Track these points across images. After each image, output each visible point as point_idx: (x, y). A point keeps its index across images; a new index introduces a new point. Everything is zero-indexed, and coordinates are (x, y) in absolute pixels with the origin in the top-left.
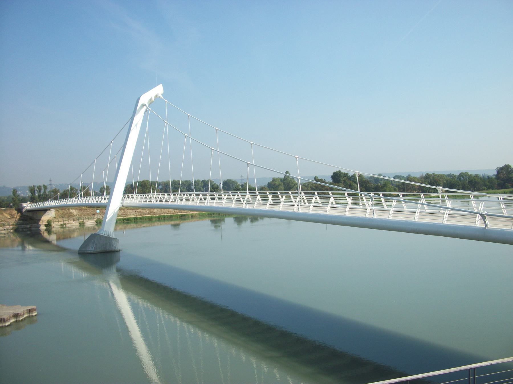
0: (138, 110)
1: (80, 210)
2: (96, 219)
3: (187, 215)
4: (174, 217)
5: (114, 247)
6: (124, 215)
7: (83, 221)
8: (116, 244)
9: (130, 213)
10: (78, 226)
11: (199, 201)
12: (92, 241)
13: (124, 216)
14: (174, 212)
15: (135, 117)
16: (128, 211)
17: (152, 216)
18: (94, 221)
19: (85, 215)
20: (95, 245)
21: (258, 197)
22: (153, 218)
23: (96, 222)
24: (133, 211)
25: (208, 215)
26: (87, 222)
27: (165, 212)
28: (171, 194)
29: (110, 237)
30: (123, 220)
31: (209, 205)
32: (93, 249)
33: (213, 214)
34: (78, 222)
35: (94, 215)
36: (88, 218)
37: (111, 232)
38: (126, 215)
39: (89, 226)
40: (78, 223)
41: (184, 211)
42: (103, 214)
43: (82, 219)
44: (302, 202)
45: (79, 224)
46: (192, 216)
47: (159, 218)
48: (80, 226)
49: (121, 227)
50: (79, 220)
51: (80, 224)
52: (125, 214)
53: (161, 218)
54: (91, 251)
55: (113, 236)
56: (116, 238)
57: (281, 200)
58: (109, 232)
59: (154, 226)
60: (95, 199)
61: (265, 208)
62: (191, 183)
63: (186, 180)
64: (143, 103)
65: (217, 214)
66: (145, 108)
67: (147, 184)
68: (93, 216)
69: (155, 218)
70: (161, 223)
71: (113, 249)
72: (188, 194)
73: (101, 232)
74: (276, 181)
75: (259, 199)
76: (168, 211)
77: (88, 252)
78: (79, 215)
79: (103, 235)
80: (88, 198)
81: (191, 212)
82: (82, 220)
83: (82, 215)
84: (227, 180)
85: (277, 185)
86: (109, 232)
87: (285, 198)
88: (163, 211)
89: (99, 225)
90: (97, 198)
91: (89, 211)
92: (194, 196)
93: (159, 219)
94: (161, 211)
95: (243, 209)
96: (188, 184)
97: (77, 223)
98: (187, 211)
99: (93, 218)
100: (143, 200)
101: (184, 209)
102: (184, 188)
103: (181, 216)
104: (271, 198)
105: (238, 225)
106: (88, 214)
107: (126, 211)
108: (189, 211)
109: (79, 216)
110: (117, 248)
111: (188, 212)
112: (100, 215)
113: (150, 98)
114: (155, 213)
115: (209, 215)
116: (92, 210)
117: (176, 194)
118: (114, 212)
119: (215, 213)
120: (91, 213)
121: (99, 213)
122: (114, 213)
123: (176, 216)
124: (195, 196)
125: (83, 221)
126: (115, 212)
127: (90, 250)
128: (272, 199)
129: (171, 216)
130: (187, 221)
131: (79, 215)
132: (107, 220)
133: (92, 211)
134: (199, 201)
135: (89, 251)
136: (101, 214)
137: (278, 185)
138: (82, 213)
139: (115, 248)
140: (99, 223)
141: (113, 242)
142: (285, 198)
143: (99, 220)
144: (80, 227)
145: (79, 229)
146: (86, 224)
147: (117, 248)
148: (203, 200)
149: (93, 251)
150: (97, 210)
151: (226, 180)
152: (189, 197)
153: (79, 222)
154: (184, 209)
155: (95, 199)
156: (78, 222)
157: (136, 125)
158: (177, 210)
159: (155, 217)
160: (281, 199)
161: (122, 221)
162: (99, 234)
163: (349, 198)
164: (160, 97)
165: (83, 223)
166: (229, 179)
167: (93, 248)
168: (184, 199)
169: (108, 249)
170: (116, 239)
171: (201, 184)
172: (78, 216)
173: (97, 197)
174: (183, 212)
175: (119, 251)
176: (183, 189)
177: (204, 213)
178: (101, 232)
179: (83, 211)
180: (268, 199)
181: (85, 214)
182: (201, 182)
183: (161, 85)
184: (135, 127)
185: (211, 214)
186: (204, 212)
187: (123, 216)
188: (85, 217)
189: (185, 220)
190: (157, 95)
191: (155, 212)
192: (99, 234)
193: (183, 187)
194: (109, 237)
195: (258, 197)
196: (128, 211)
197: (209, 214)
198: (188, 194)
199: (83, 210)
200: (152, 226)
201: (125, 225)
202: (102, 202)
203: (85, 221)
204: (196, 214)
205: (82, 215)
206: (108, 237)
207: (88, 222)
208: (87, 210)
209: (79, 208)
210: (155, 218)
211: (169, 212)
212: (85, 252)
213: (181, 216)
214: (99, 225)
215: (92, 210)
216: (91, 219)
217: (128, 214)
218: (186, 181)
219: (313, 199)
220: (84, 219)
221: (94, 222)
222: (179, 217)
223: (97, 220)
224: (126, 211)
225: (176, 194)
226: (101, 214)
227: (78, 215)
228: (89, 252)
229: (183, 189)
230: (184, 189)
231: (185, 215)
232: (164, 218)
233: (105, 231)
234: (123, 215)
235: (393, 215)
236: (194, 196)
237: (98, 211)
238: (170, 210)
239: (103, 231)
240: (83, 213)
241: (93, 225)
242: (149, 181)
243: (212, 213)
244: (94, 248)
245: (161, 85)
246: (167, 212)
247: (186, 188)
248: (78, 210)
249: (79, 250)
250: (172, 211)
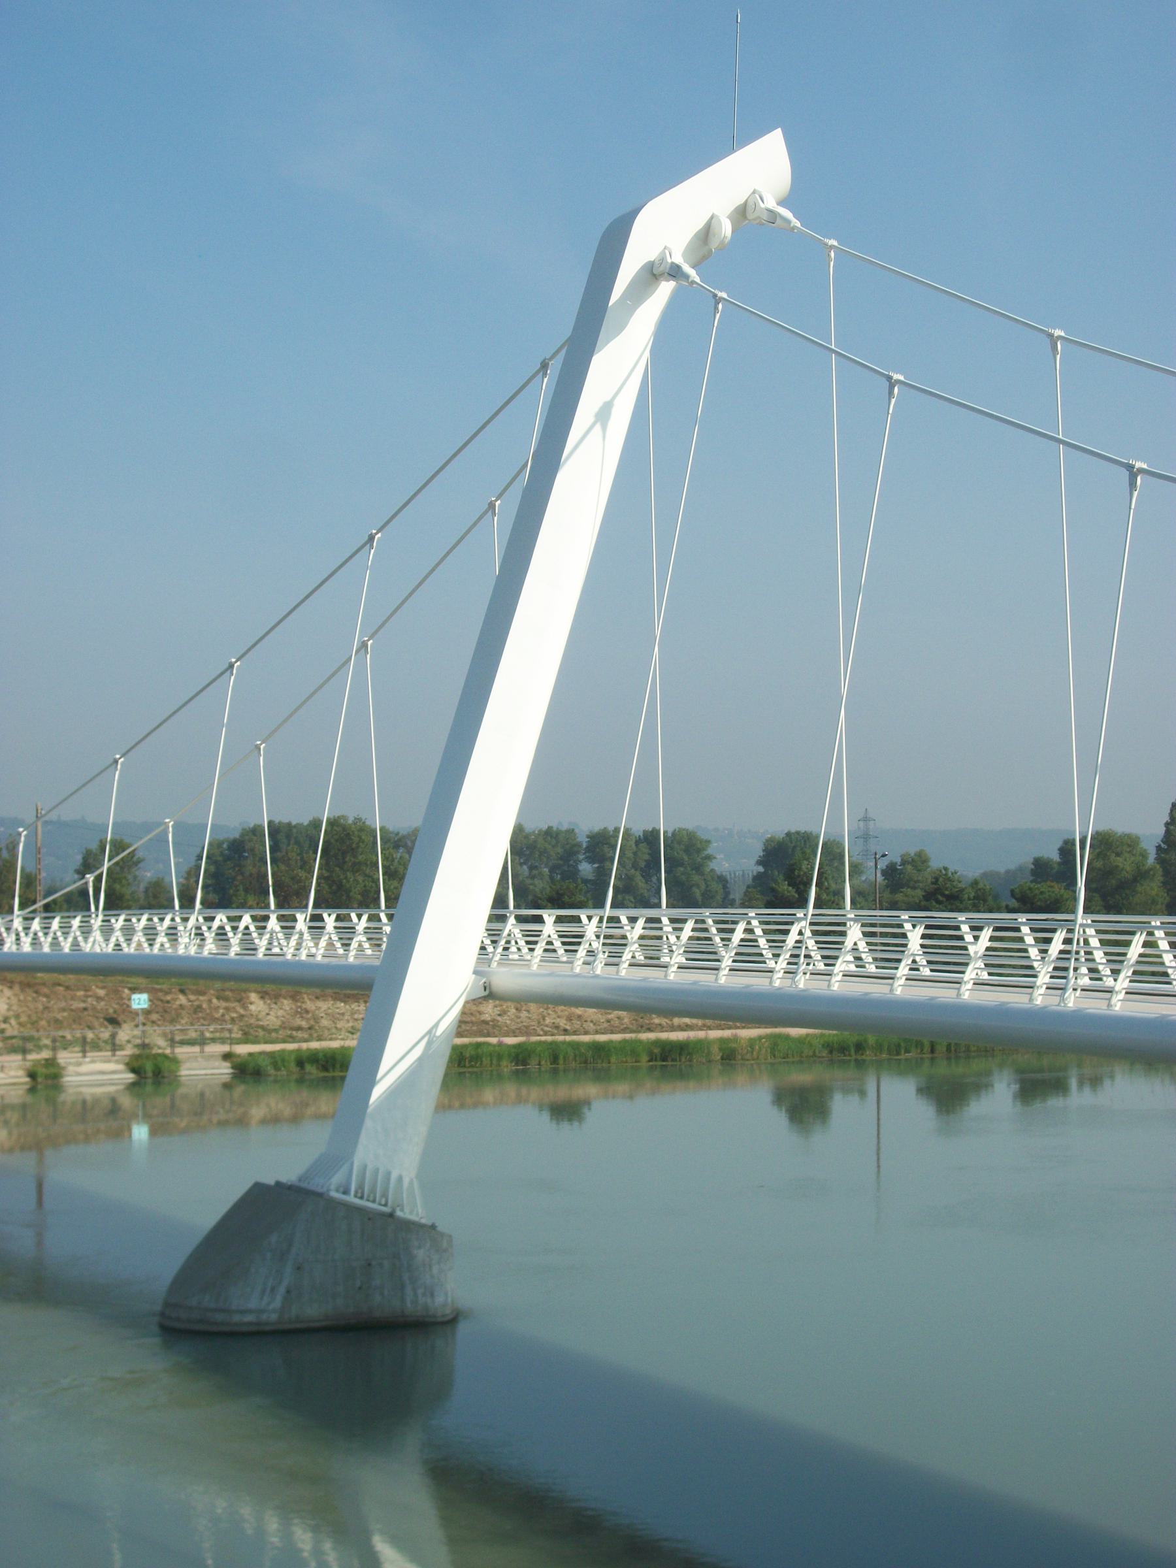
0: (611, 306)
1: (29, 985)
2: (129, 1051)
3: (701, 1045)
4: (613, 1059)
5: (420, 1291)
6: (299, 1028)
7: (51, 1063)
8: (435, 1270)
9: (334, 1018)
10: (21, 1092)
11: (1126, 984)
12: (274, 1238)
13: (299, 1034)
14: (606, 1025)
15: (593, 358)
16: (324, 1006)
17: (478, 1045)
18: (117, 1062)
19: (58, 1023)
20: (289, 1269)
21: (854, 934)
22: (486, 1061)
23: (133, 1070)
24: (354, 1006)
25: (825, 1053)
26: (79, 1064)
27: (548, 1021)
28: (908, 926)
29: (399, 1213)
30: (300, 1063)
31: (801, 986)
32: (277, 1303)
33: (860, 1047)
34: (20, 1068)
35: (114, 1021)
36: (85, 1046)
37: (400, 1179)
38: (313, 1032)
39: (88, 1092)
40: (21, 1073)
41: (664, 1021)
42: (167, 1016)
43: (39, 1048)
44: (1084, 970)
45: (27, 1079)
46: (730, 1056)
47: (521, 1056)
48: (32, 1090)
49: (273, 1105)
50: (24, 1051)
51: (32, 1075)
52: (304, 1024)
53: (533, 1062)
54: (264, 1317)
55: (415, 1210)
56: (429, 1223)
57: (972, 949)
58: (368, 1175)
59: (476, 1105)
60: (66, 934)
61: (886, 989)
62: (579, 845)
63: (550, 828)
64: (652, 256)
65: (879, 1047)
66: (666, 288)
67: (356, 839)
68: (110, 1028)
69: (500, 1057)
70: (524, 1091)
71: (412, 1303)
72: (755, 923)
73: (337, 1179)
74: (1118, 855)
75: (855, 944)
76: (569, 1019)
77: (236, 1318)
78: (23, 1019)
79: (351, 1199)
80: (57, 920)
81: (709, 1028)
82: (45, 1054)
83: (43, 1023)
84: (788, 834)
85: (1124, 874)
86: (389, 1174)
87: (643, 928)
88: (535, 1017)
89: (149, 1088)
90: (55, 924)
91: (81, 993)
92: (749, 931)
93: (525, 1063)
94: (524, 1014)
95: (1042, 1014)
96: (560, 850)
97: (13, 1073)
98: (687, 1020)
99: (114, 1046)
100: (627, 956)
101: (670, 1011)
102: (535, 872)
103: (657, 1051)
104: (921, 941)
105: (937, 1111)
106: (78, 1018)
107: (309, 1005)
108: (700, 1022)
109: (20, 1024)
110: (440, 1299)
111: (687, 1028)
112: (153, 1022)
113: (700, 224)
114: (485, 1022)
115: (831, 1052)
116: (101, 992)
117: (965, 928)
118: (429, 1032)
119: (871, 1039)
120: (94, 1008)
121: (147, 1012)
122: (429, 1043)
123: (630, 1050)
124: (808, 933)
125: (51, 1063)
126: (439, 1033)
127: (253, 1304)
128: (922, 946)
129: (599, 1049)
130: (692, 1084)
131: (23, 1019)
132: (377, 1092)
133: (99, 999)
134: (1126, 984)
135: (250, 1311)
136: (154, 1017)
137: (1130, 877)
138: (41, 1007)
139: (429, 1300)
140: (150, 1074)
141: (420, 1254)
142: (643, 928)
143: (148, 1057)
144: (29, 1099)
145: (24, 1107)
146: (69, 1079)
147: (440, 1299)
148: (561, 951)
149: (274, 1317)
150: (135, 990)
151: (780, 835)
152: (1034, 952)
153: (28, 1064)
154: (670, 1011)
155: (66, 934)
156: (20, 1068)
157: (604, 415)
158: (623, 1014)
159: (499, 1054)
160: (969, 947)
161: (293, 1067)
162: (320, 1190)
163: (329, 915)
164: (773, 216)
165: (52, 1070)
166: (798, 833)
167: (273, 1289)
168: (163, 934)
169: (383, 1302)
170: (433, 1227)
171: (635, 854)
172: (13, 1022)
173: (78, 919)
174: (661, 1028)
175: (452, 1321)
176: (529, 881)
177: (801, 1040)
178: (337, 1179)
179: (47, 996)
180: (905, 945)
181: (59, 1016)
182: (638, 842)
183: (779, 131)
184: (598, 427)
185: (843, 1049)
186: (802, 1031)
187: (292, 1039)
188: (61, 1033)
189: (683, 1076)
190: (745, 204)
191: (487, 1017)
192: (320, 1195)
193: (531, 868)
194: (391, 1215)
195: (854, 934)
196: (320, 1004)
197: (830, 1047)
198: (1159, 934)
199: (46, 990)
200: (462, 1106)
201: (305, 1094)
202: (87, 947)
203: (63, 1057)
204: (752, 1042)
205: (43, 1023)
206: (382, 1214)
207: (84, 1068)
208: (68, 988)
209: (20, 977)
210: (500, 1057)
211: (577, 1024)
212: (219, 1317)
213: (657, 1051)
214: (149, 1088)
215: (101, 992)
216: (96, 1047)
217: (325, 1022)
218: (549, 833)
219: (1054, 941)
220: (54, 1049)
221: (121, 1067)
222: (644, 1058)
223: (136, 1057)
224: (309, 1005)
225: (965, 928)
226: (154, 1017)
227: (17, 1016)
228: (249, 1318)
229: (529, 881)
230: (536, 881)
231: (682, 1048)
232: (555, 1059)
233: (365, 1167)
234: (292, 1029)
235: (726, 979)
236: (800, 933)
237: (140, 1001)
238: (579, 1011)
239: (344, 1170)
240: (46, 1008)
241: (112, 1089)
242: (373, 826)
243: (851, 1038)
244: (282, 1290)
245: (779, 131)
246: (562, 1023)
247: (546, 870)
248: (17, 988)
249: (167, 1304)
250: (594, 1017)
